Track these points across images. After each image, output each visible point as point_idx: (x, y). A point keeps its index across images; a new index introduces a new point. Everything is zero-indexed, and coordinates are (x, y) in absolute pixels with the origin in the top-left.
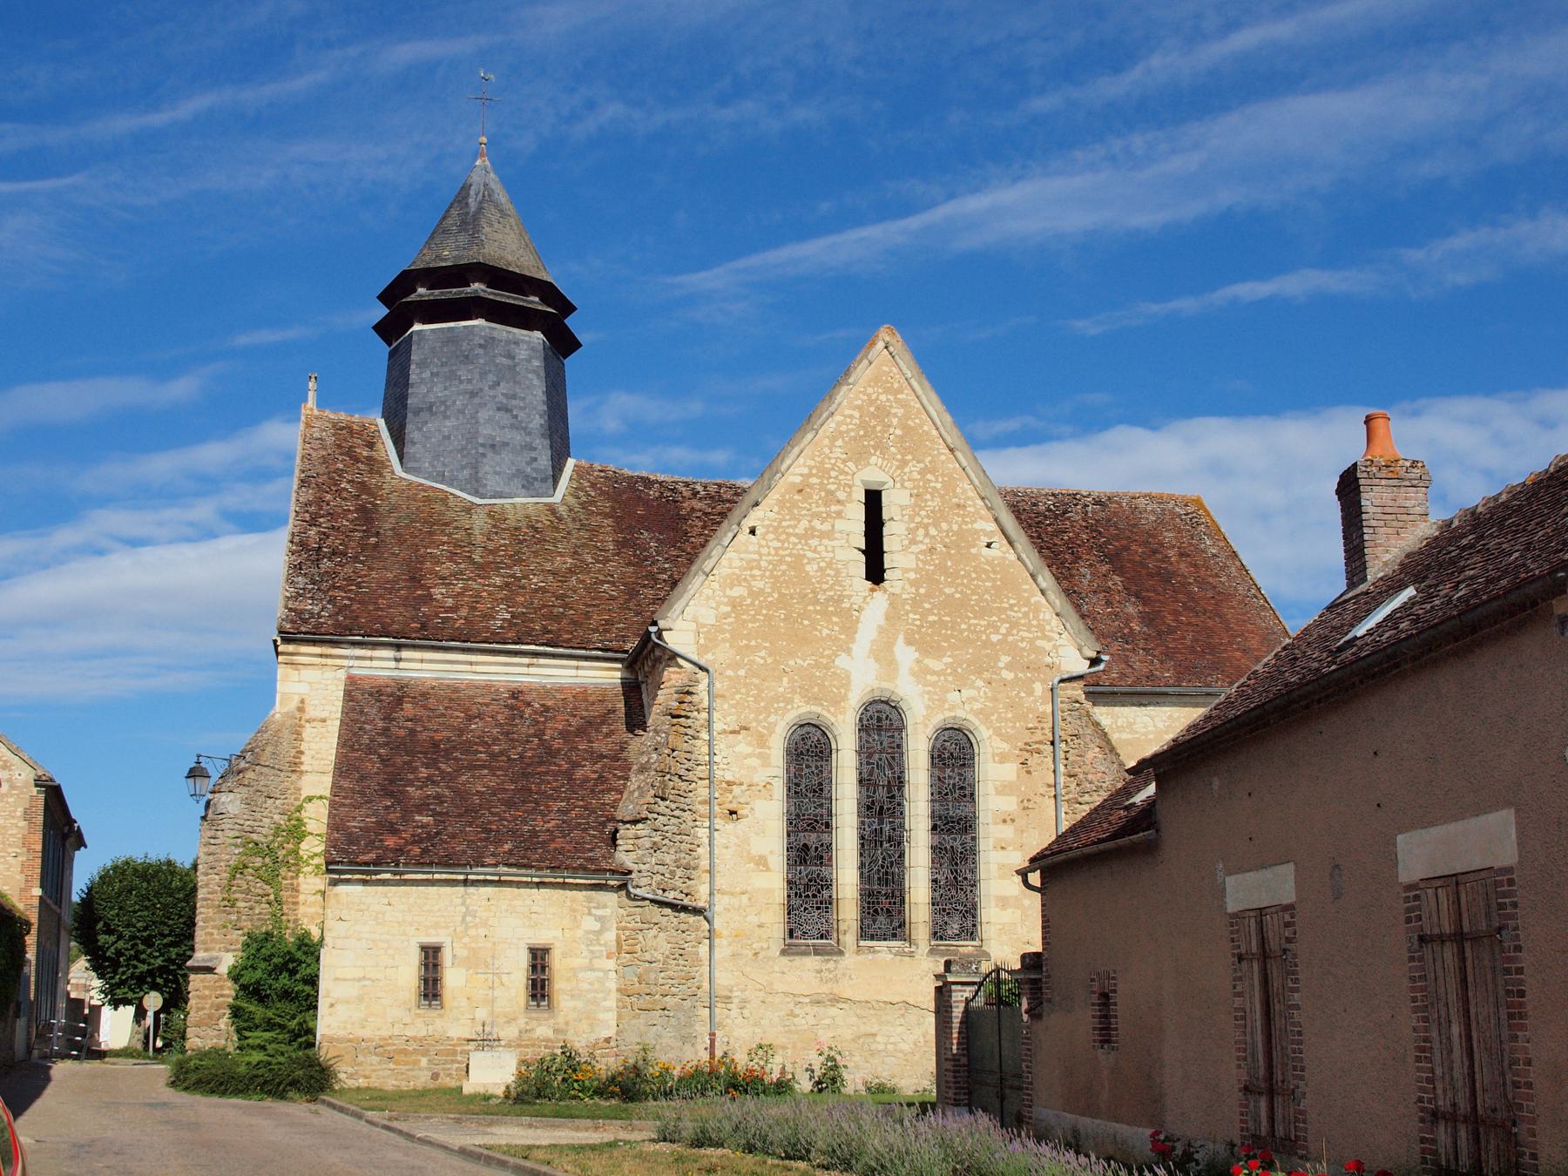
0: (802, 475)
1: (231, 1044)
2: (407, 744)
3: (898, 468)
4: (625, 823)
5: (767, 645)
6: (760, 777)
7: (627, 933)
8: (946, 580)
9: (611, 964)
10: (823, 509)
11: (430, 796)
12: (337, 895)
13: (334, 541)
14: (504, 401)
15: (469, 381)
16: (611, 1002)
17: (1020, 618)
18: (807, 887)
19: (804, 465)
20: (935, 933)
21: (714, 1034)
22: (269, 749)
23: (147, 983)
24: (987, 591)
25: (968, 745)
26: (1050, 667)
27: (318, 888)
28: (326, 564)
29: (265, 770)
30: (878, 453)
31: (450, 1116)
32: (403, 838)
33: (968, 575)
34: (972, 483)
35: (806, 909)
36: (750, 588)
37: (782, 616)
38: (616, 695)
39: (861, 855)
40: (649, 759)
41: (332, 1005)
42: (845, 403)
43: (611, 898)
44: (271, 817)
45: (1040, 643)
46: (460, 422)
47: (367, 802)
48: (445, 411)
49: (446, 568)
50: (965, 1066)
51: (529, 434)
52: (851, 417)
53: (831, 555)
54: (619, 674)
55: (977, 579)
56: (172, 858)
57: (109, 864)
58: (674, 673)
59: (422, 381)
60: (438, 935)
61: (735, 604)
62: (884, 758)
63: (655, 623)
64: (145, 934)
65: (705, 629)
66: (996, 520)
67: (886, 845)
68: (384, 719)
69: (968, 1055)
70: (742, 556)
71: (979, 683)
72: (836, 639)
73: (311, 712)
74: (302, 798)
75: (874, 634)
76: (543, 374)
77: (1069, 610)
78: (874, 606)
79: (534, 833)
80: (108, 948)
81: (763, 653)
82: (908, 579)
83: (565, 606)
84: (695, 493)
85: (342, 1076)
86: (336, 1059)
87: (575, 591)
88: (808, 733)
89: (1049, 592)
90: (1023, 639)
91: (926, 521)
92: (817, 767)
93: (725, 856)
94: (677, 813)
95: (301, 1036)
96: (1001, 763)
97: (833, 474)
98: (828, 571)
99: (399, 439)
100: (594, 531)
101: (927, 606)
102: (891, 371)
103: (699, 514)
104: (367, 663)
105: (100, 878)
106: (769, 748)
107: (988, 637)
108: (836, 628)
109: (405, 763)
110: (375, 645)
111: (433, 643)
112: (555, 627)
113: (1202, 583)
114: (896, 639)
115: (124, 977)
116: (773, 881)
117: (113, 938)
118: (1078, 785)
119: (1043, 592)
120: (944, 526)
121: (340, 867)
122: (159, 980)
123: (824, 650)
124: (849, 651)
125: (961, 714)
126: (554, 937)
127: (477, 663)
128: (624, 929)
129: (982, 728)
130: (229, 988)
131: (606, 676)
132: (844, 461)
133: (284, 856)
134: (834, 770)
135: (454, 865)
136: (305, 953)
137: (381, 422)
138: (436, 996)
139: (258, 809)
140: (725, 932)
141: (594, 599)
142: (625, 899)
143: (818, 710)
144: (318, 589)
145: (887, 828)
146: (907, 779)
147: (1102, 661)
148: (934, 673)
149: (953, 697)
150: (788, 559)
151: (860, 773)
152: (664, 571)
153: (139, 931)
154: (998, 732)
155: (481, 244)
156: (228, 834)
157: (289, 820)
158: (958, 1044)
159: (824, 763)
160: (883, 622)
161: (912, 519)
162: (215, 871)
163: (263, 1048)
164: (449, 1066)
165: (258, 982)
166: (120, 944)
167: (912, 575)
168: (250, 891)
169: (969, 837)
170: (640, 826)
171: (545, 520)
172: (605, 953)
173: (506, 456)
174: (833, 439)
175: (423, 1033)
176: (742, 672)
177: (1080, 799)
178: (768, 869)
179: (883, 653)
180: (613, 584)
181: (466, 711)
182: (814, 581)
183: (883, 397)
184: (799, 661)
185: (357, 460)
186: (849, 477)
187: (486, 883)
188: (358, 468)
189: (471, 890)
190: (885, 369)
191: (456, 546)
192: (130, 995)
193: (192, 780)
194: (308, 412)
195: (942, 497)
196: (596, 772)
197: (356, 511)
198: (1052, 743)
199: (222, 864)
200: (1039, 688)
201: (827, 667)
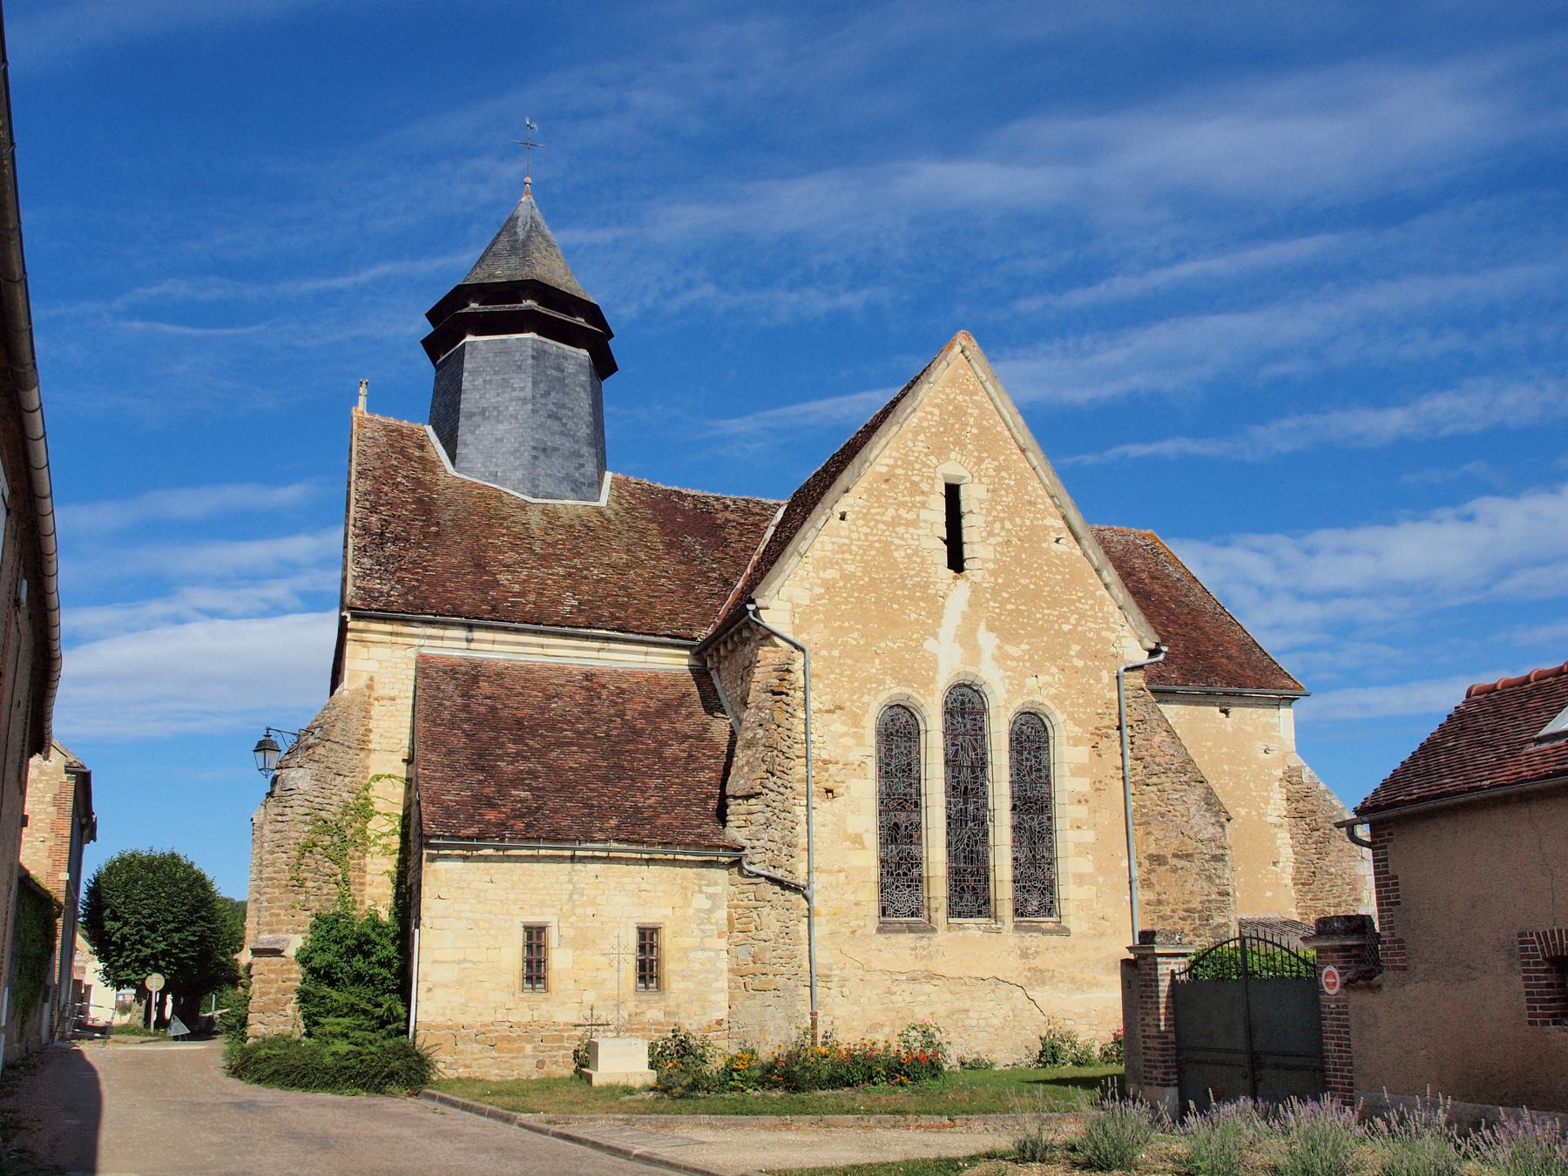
0: (888, 465)
1: (299, 1031)
2: (491, 720)
3: (975, 464)
4: (736, 798)
5: (859, 627)
6: (855, 755)
7: (740, 911)
8: (1021, 571)
9: (723, 943)
10: (908, 499)
11: (522, 771)
12: (435, 871)
13: (396, 528)
14: (555, 410)
15: (522, 389)
16: (723, 983)
17: (1087, 610)
18: (899, 865)
19: (890, 457)
20: (1017, 910)
21: (816, 1014)
22: (339, 725)
23: (150, 966)
24: (1057, 584)
25: (1043, 729)
26: (1115, 656)
27: (385, 868)
28: (390, 548)
29: (335, 746)
30: (957, 449)
31: (617, 1116)
32: (504, 813)
33: (1040, 568)
34: (1041, 481)
35: (897, 887)
36: (842, 570)
37: (873, 600)
38: (687, 680)
39: (948, 834)
40: (755, 735)
41: (430, 990)
42: (926, 400)
43: (721, 875)
44: (340, 794)
45: (1104, 633)
46: (513, 426)
47: (458, 776)
48: (498, 416)
49: (510, 557)
50: (1172, 1043)
51: (577, 442)
52: (932, 414)
53: (917, 543)
54: (686, 661)
55: (1050, 571)
56: (175, 851)
57: (116, 856)
58: (769, 651)
59: (475, 388)
60: (543, 914)
61: (828, 586)
62: (967, 741)
63: (752, 601)
64: (149, 921)
65: (800, 610)
66: (1064, 518)
67: (970, 824)
68: (463, 696)
69: (1177, 1032)
70: (834, 539)
71: (1054, 670)
72: (924, 623)
73: (380, 691)
74: (370, 777)
75: (959, 621)
76: (589, 389)
77: (1130, 603)
78: (957, 593)
79: (637, 810)
80: (114, 933)
81: (855, 635)
82: (988, 569)
83: (629, 596)
84: (727, 507)
85: (440, 1066)
86: (438, 1047)
87: (635, 584)
88: (897, 714)
89: (1112, 586)
90: (1090, 630)
91: (1002, 515)
92: (905, 748)
93: (822, 834)
94: (782, 790)
95: (390, 1024)
96: (1076, 746)
97: (917, 466)
98: (914, 559)
99: (450, 443)
100: (643, 533)
101: (1005, 595)
102: (966, 374)
103: (734, 524)
104: (438, 643)
105: (107, 869)
106: (863, 728)
107: (1060, 625)
108: (923, 613)
109: (492, 738)
110: (454, 624)
111: (506, 624)
112: (622, 614)
113: (1177, 602)
114: (978, 625)
115: (128, 961)
116: (867, 859)
117: (118, 925)
118: (1145, 767)
119: (1107, 586)
120: (1018, 520)
121: (441, 841)
122: (162, 963)
123: (913, 634)
124: (935, 635)
125: (1039, 699)
126: (665, 916)
127: (548, 646)
128: (736, 907)
129: (1058, 713)
130: (297, 972)
131: (673, 662)
132: (926, 455)
133: (352, 835)
134: (922, 752)
135: (562, 840)
136: (379, 935)
137: (429, 429)
138: (540, 979)
139: (327, 786)
140: (823, 911)
141: (654, 591)
142: (737, 877)
143: (909, 691)
144: (385, 570)
145: (971, 807)
146: (989, 760)
147: (1162, 651)
148: (1013, 659)
149: (1031, 682)
150: (877, 545)
151: (946, 755)
152: (714, 570)
153: (144, 917)
154: (1071, 717)
155: (531, 266)
156: (298, 809)
157: (358, 799)
158: (1166, 1020)
159: (913, 744)
160: (965, 608)
161: (989, 513)
162: (283, 849)
163: (346, 1036)
164: (555, 1053)
165: (330, 965)
166: (126, 930)
167: (991, 566)
168: (319, 870)
169: (1045, 817)
170: (753, 801)
171: (595, 521)
172: (716, 932)
173: (557, 460)
174: (916, 434)
175: (529, 1018)
176: (836, 653)
177: (1147, 781)
178: (864, 848)
179: (967, 638)
180: (669, 578)
181: (543, 690)
182: (901, 566)
183: (960, 398)
184: (889, 644)
185: (410, 459)
186: (932, 470)
187: (594, 859)
188: (411, 466)
189: (579, 866)
190: (960, 371)
191: (515, 538)
192: (133, 977)
193: (261, 754)
194: (360, 415)
195: (1015, 493)
196: (685, 751)
197: (414, 502)
198: (1119, 728)
199: (291, 842)
200: (1106, 677)
201: (915, 649)
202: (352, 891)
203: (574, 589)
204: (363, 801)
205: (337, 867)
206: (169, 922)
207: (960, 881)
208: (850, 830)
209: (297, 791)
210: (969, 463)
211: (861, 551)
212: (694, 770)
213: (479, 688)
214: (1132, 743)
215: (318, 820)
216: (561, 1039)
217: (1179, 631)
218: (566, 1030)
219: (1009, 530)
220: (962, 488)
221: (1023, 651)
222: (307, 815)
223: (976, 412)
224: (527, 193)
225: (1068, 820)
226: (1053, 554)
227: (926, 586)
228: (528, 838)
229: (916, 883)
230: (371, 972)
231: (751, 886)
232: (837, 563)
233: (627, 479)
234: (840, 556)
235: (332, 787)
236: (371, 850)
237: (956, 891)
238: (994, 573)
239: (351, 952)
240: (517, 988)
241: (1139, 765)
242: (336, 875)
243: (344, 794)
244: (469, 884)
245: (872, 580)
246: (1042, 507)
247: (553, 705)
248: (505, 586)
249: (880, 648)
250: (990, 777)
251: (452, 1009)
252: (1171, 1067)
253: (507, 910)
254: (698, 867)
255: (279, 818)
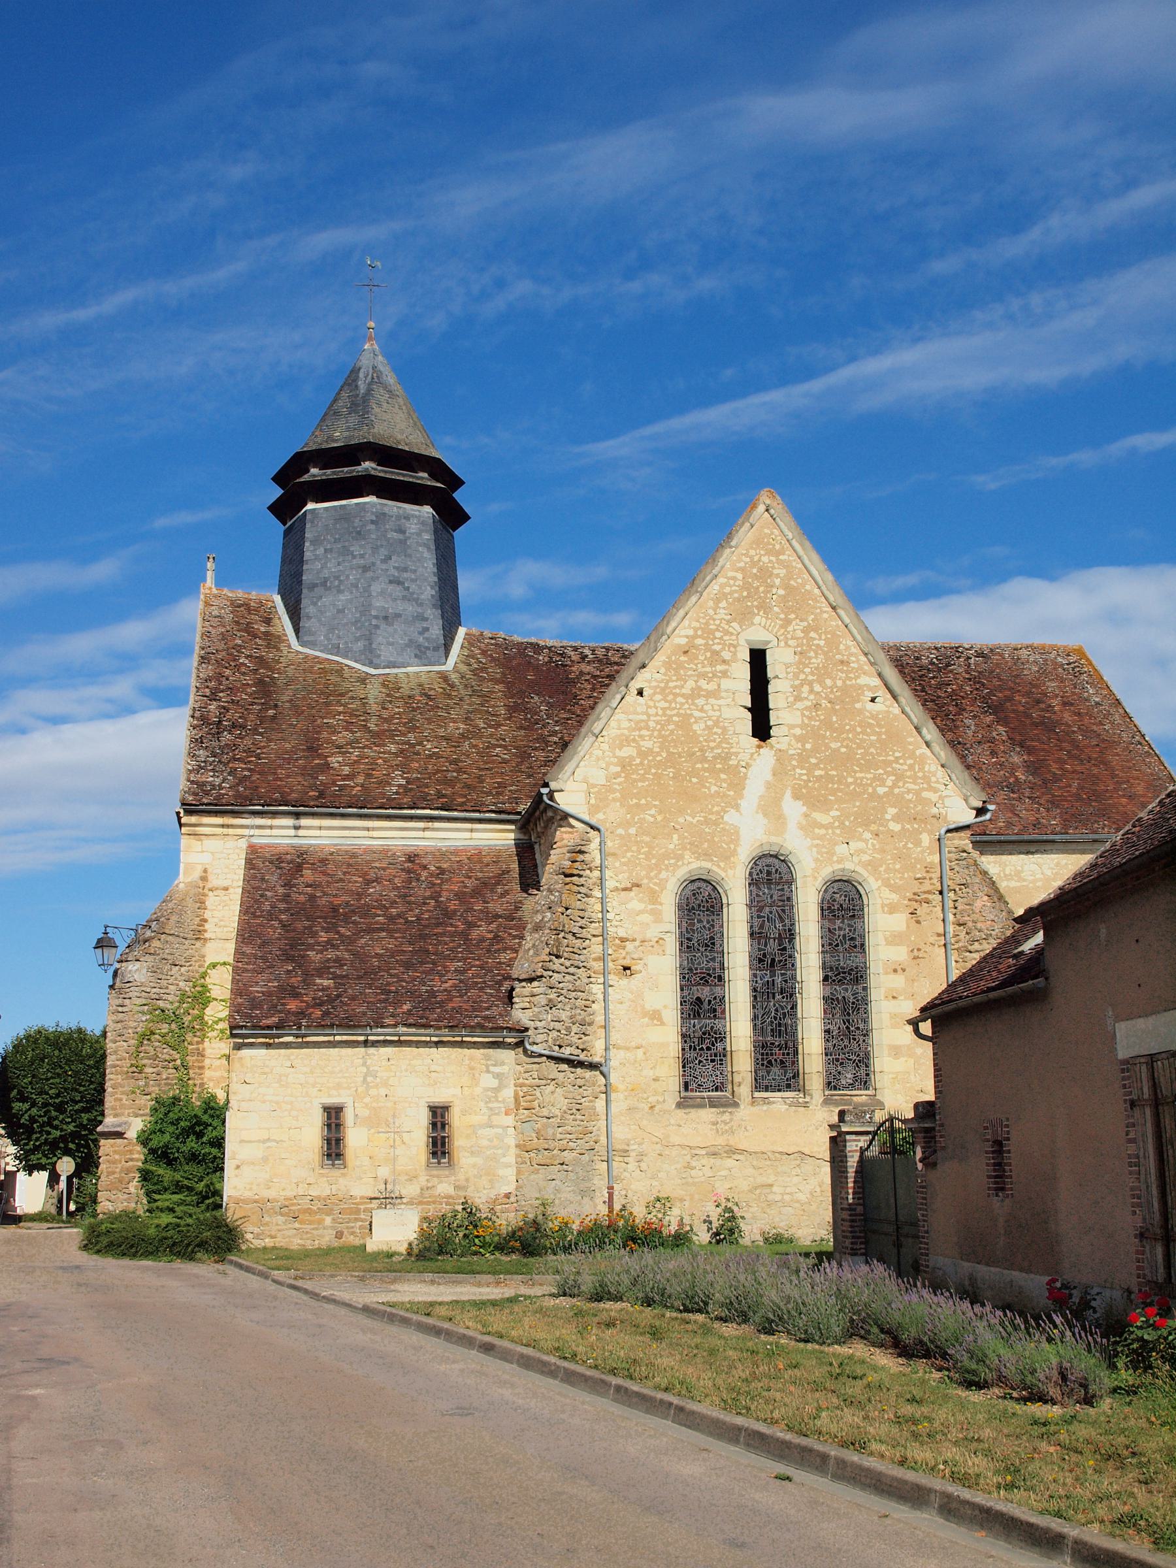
0: (687, 637)
2: (308, 911)
3: (781, 627)
4: (520, 981)
5: (657, 803)
7: (525, 1089)
8: (831, 735)
9: (510, 1120)
10: (708, 669)
11: (330, 959)
13: (234, 714)
14: (396, 574)
15: (362, 556)
16: (511, 1158)
18: (702, 1040)
19: (690, 627)
20: (829, 1083)
22: (174, 918)
23: (60, 1148)
25: (857, 896)
26: (937, 817)
27: (222, 1053)
28: (226, 737)
30: (761, 613)
33: (853, 730)
34: (855, 639)
35: (700, 1062)
36: (638, 747)
37: (671, 775)
39: (754, 1007)
41: (238, 1167)
43: (508, 1056)
44: (178, 983)
45: (925, 794)
48: (339, 586)
49: (343, 737)
51: (421, 605)
52: (734, 578)
53: (718, 713)
54: (512, 836)
56: (82, 1025)
57: (22, 1033)
58: (566, 833)
59: (317, 558)
60: (339, 1095)
61: (624, 764)
63: (546, 785)
65: (596, 789)
66: (880, 675)
67: (778, 997)
68: (285, 885)
71: (867, 835)
72: (725, 795)
73: (214, 881)
76: (433, 547)
77: (954, 761)
79: (432, 993)
80: (22, 1115)
81: (653, 812)
83: (459, 771)
84: (584, 657)
85: (249, 1236)
88: (699, 888)
90: (909, 791)
91: (810, 678)
92: (708, 922)
94: (572, 970)
96: (891, 913)
97: (718, 635)
98: (715, 730)
101: (813, 761)
102: (772, 533)
103: (588, 677)
104: (268, 832)
106: (661, 904)
107: (874, 789)
108: (724, 785)
109: (305, 928)
110: (275, 814)
112: (448, 791)
113: (1086, 731)
117: (26, 1106)
118: (967, 933)
119: (928, 744)
120: (829, 682)
121: (244, 1031)
122: (71, 1146)
124: (737, 807)
125: (849, 866)
126: (454, 1095)
127: (374, 829)
129: (871, 880)
130: (139, 1153)
132: (728, 622)
134: (725, 925)
135: (355, 1026)
136: (212, 1116)
137: (278, 599)
138: (339, 1155)
140: (621, 1087)
143: (708, 865)
144: (220, 761)
145: (778, 979)
146: (797, 931)
148: (822, 826)
149: (841, 849)
150: (676, 719)
151: (751, 927)
152: (555, 733)
153: (51, 1098)
154: (887, 884)
155: (371, 425)
156: (135, 1001)
157: (194, 987)
158: (854, 1193)
159: (715, 917)
160: (769, 777)
161: (796, 676)
162: (124, 1038)
165: (166, 1146)
166: (34, 1111)
167: (798, 731)
169: (860, 987)
170: (535, 984)
172: (503, 1110)
173: (398, 626)
174: (717, 601)
175: (328, 1192)
176: (632, 831)
177: (970, 948)
178: (662, 1024)
179: (771, 808)
180: (505, 747)
182: (701, 739)
183: (765, 559)
184: (689, 818)
185: (255, 636)
186: (734, 637)
187: (386, 1043)
188: (256, 643)
189: (372, 1050)
190: (766, 531)
191: (351, 715)
195: (825, 654)
197: (254, 685)
198: (941, 893)
199: (130, 1031)
200: (926, 839)
202: (192, 1075)
203: (404, 767)
204: (200, 989)
205: (175, 1052)
206: (76, 1102)
207: (767, 1054)
208: (648, 1007)
209: (135, 984)
210: (774, 626)
211: (659, 726)
212: (496, 951)
213: (302, 876)
214: (956, 908)
215: (155, 1010)
216: (358, 1211)
217: (1078, 768)
218: (362, 1204)
219: (818, 693)
220: (768, 653)
221: (833, 817)
222: (144, 1005)
223: (783, 572)
224: (370, 339)
225: (883, 990)
226: (867, 714)
227: (726, 757)
228: (323, 1026)
229: (721, 1057)
230: (203, 1152)
231: (534, 1066)
232: (634, 740)
233: (482, 634)
234: (637, 733)
235: (168, 977)
236: (209, 1035)
237: (763, 1065)
238: (801, 739)
239: (186, 1133)
240: (317, 1164)
241: (962, 932)
242: (175, 1060)
243: (181, 983)
244: (272, 1070)
245: (670, 754)
246: (855, 665)
247: (371, 890)
248: (335, 770)
249: (678, 823)
250: (798, 949)
251: (258, 1185)
252: (859, 1238)
253: (307, 1092)
254: (484, 1048)
255: (120, 1009)
